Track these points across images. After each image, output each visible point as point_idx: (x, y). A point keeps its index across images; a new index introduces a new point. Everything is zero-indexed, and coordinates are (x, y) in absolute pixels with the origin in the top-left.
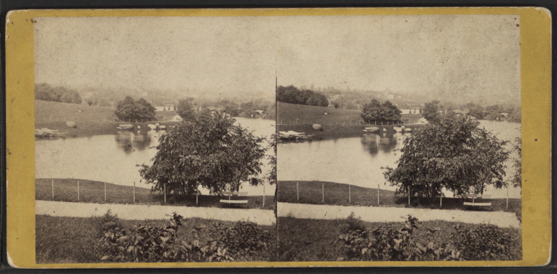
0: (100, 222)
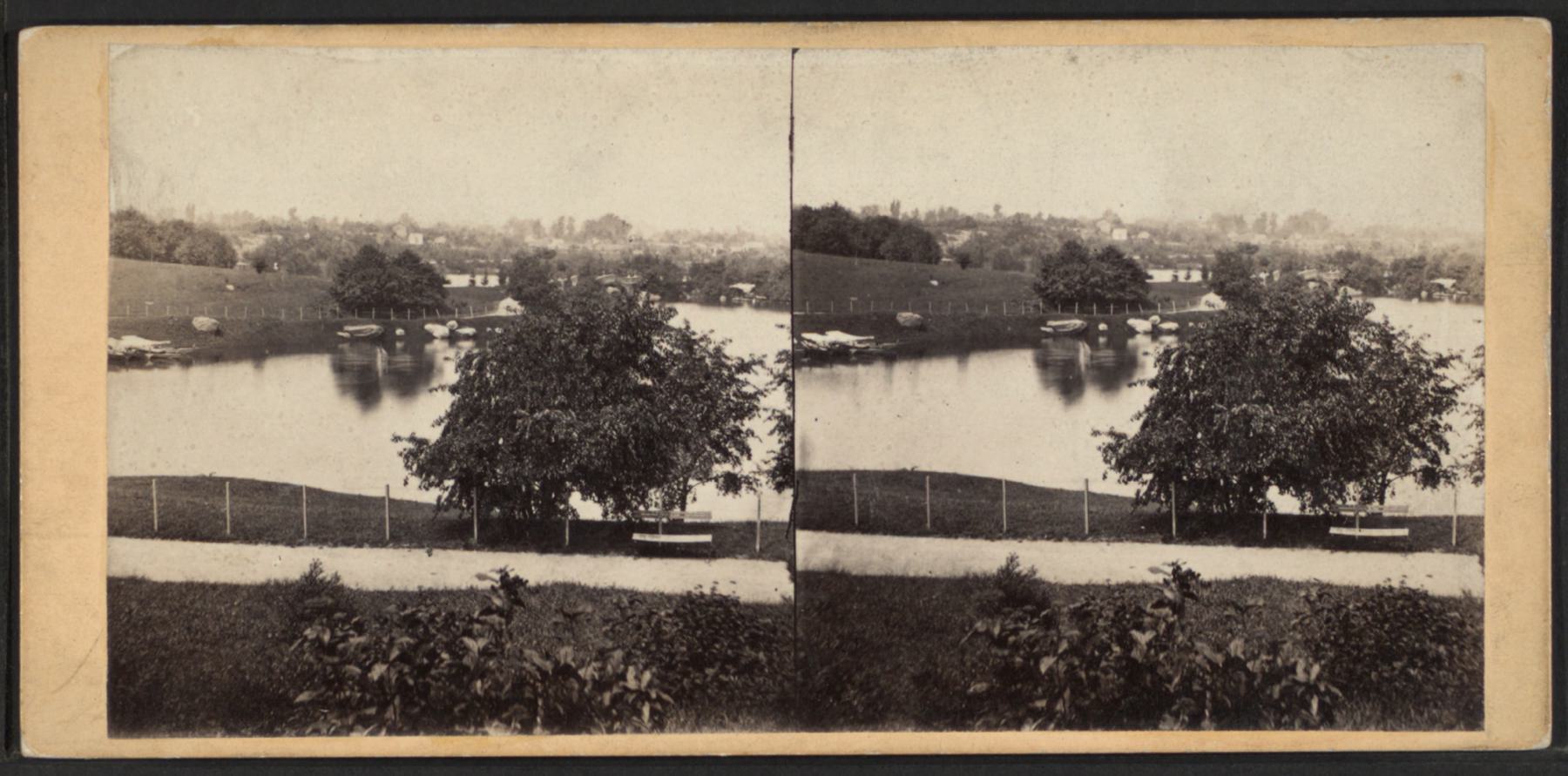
0: (291, 599)
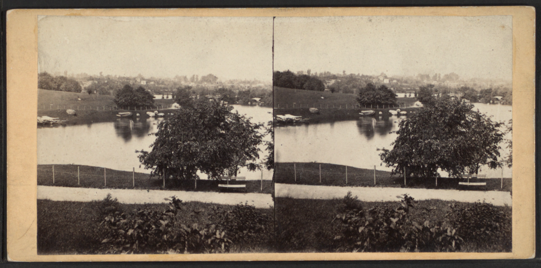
0: (100, 207)
